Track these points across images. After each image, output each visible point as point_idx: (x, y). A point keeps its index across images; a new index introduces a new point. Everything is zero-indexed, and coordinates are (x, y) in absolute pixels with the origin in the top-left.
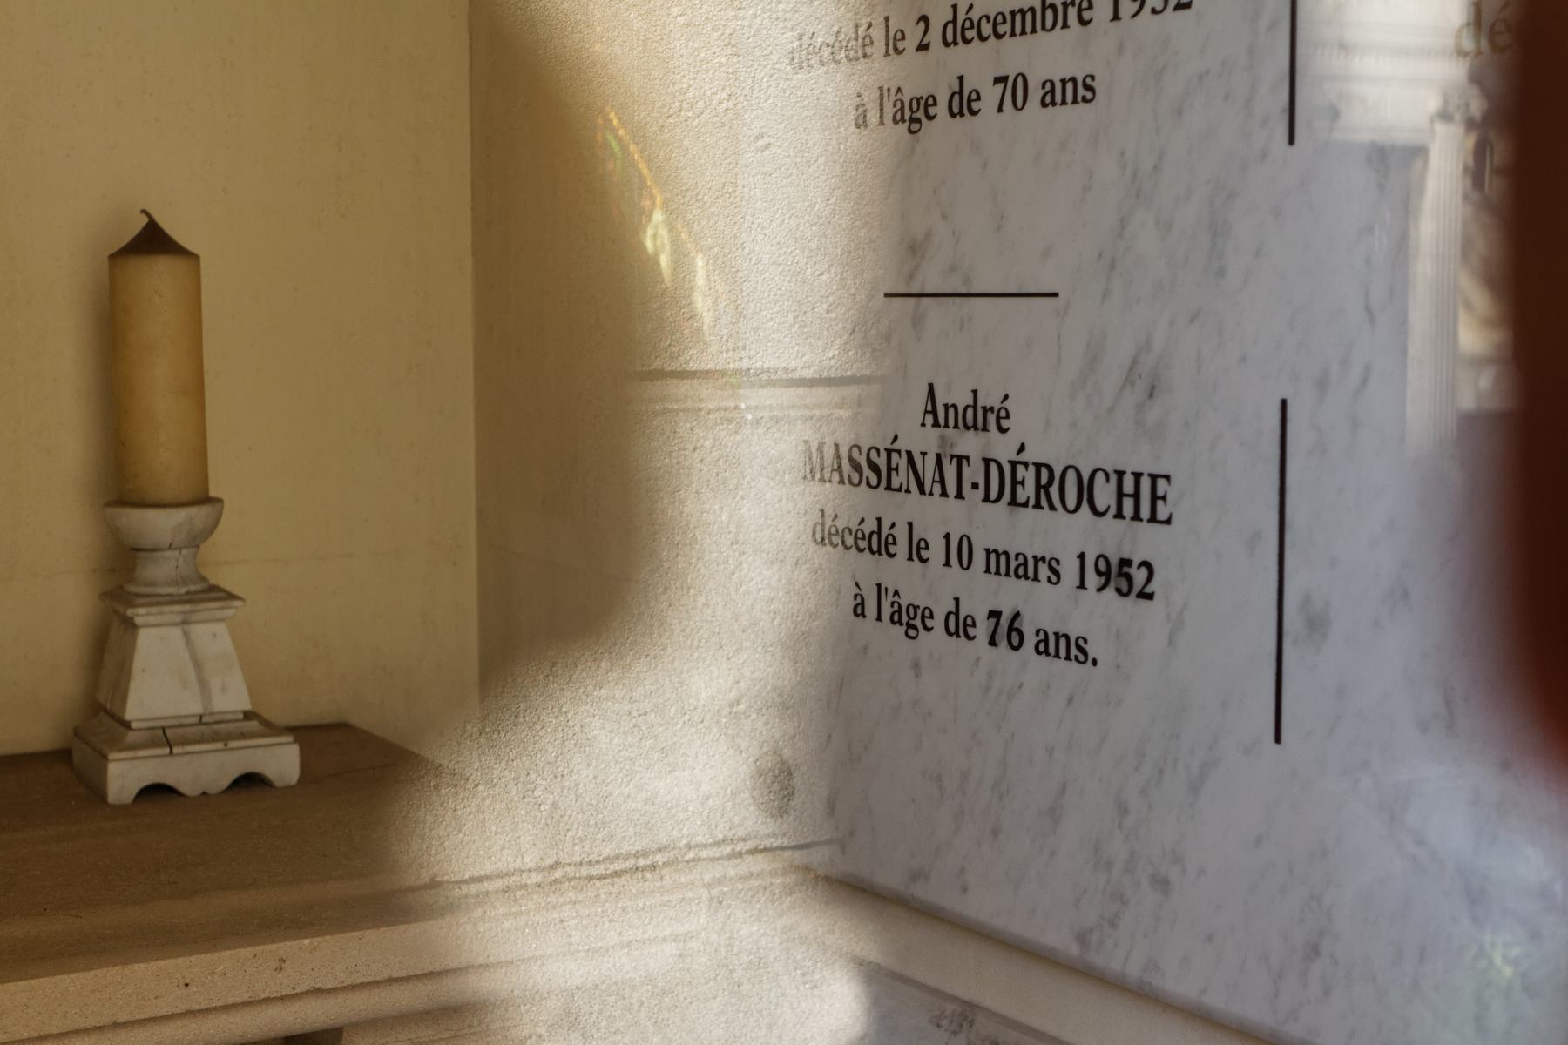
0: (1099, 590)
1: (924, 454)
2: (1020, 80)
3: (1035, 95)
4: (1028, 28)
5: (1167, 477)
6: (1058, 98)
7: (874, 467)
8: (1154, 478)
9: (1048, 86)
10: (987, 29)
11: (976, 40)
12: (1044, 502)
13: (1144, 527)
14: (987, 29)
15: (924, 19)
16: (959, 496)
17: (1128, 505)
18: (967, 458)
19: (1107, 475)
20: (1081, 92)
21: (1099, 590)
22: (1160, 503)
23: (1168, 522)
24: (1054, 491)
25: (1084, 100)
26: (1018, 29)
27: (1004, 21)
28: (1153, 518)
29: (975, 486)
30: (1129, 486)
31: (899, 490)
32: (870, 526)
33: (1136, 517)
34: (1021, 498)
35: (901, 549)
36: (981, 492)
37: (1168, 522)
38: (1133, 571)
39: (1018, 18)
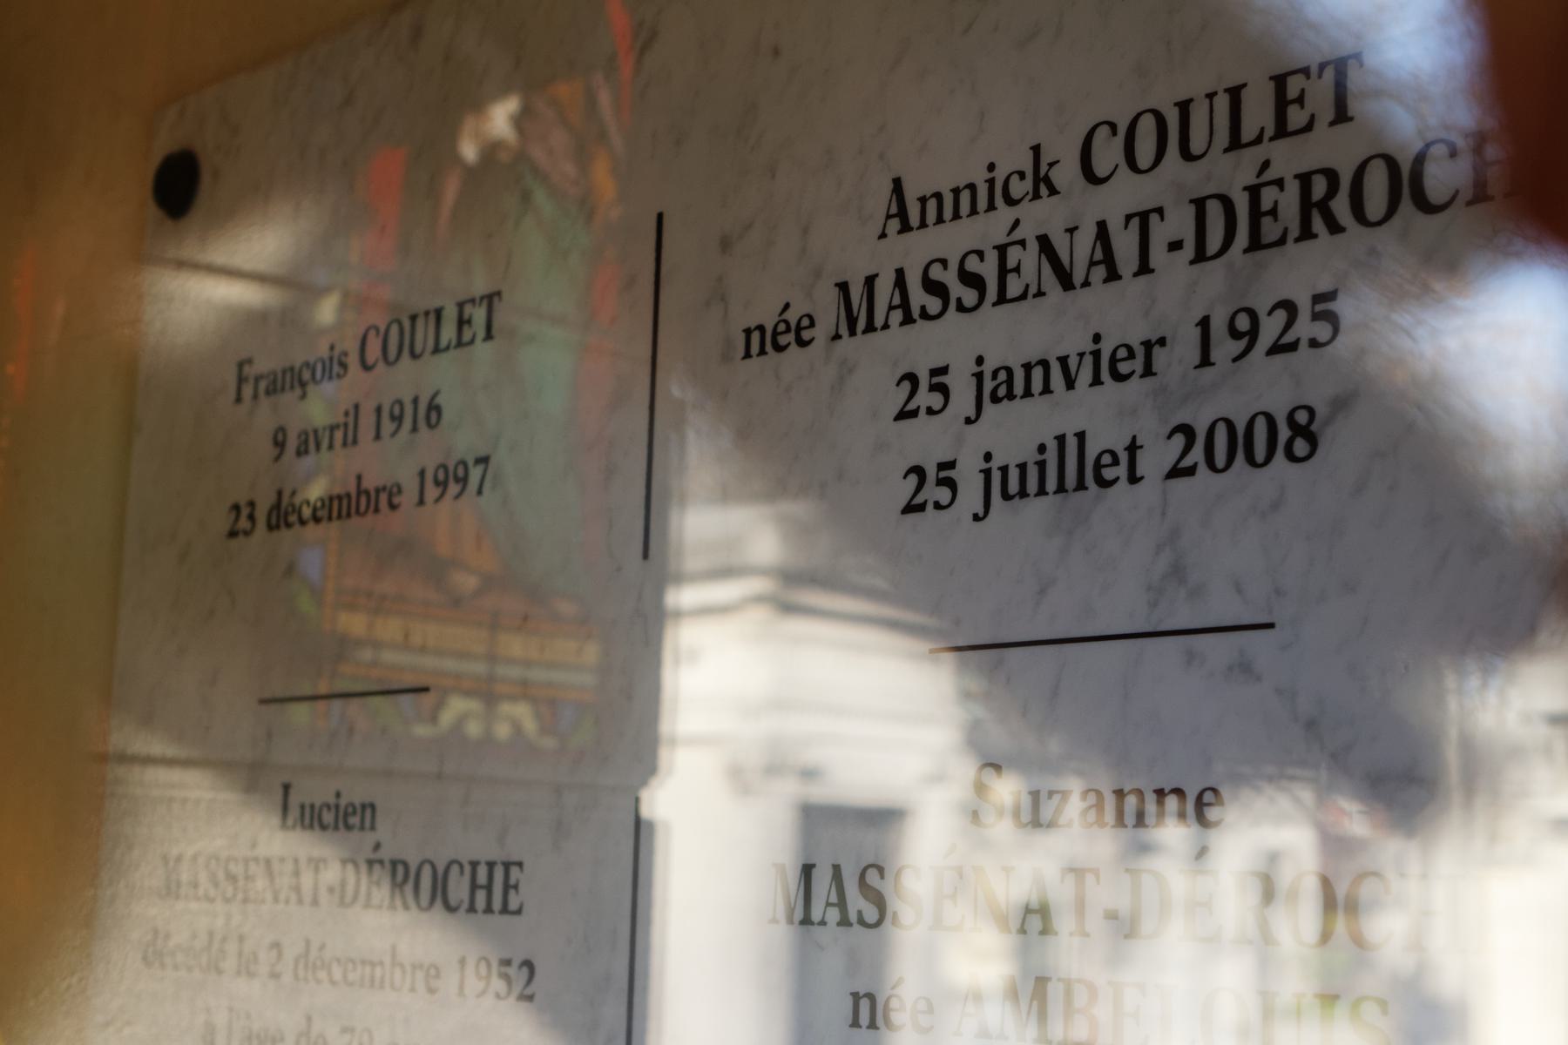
0: (479, 996)
5: (520, 864)
6: (1019, 388)
8: (507, 866)
11: (794, 346)
17: (481, 896)
18: (1160, 211)
19: (461, 866)
21: (479, 996)
23: (519, 912)
26: (335, 514)
28: (505, 910)
30: (482, 878)
33: (489, 910)
39: (336, 504)
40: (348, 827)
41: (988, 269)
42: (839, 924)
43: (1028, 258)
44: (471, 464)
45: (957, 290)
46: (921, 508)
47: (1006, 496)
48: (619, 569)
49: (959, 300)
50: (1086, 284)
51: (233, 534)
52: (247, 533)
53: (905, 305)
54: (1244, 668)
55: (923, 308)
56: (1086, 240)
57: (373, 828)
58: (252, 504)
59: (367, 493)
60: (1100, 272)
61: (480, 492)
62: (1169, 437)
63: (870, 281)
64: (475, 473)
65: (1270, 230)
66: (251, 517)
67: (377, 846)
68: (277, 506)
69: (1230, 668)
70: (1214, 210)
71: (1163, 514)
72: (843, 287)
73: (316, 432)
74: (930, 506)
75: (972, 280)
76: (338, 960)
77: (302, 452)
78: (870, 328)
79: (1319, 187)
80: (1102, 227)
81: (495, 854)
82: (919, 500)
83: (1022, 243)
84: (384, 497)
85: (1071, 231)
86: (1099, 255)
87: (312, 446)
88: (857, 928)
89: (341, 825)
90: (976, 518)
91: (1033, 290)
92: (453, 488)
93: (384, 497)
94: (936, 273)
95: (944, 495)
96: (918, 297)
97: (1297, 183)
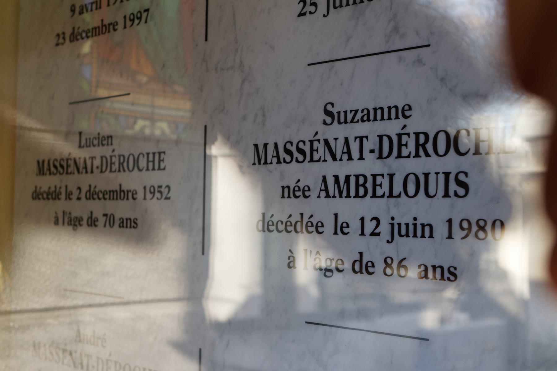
1: (336, 139)
2: (112, 217)
3: (117, 223)
4: (115, 197)
5: (164, 153)
7: (62, 166)
8: (160, 153)
9: (121, 220)
10: (101, 196)
12: (121, 169)
13: (157, 172)
14: (101, 196)
15: (79, 188)
16: (92, 172)
17: (151, 165)
18: (367, 137)
19: (143, 155)
20: (133, 224)
22: (162, 163)
23: (164, 169)
24: (125, 165)
25: (134, 227)
26: (94, 34)
27: (107, 194)
28: (159, 169)
29: (93, 367)
30: (151, 158)
31: (319, 161)
32: (53, 189)
34: (113, 169)
35: (63, 196)
36: (100, 170)
37: (164, 169)
38: (162, 189)
39: (94, 31)
40: (103, 145)
41: (307, 148)
42: (277, 163)
43: (321, 147)
44: (142, 12)
45: (296, 154)
46: (305, 14)
47: (335, 7)
48: (197, 45)
49: (297, 158)
50: (341, 160)
51: (57, 45)
52: (63, 44)
53: (278, 156)
54: (419, 61)
55: (284, 159)
56: (341, 141)
57: (112, 144)
58: (64, 33)
59: (105, 26)
60: (345, 157)
61: (146, 22)
62: (371, 221)
63: (266, 145)
64: (144, 15)
65: (405, 152)
66: (64, 38)
67: (113, 151)
68: (73, 33)
69: (414, 62)
70: (385, 140)
71: (391, 9)
72: (256, 146)
73: (86, 5)
74: (308, 13)
75: (301, 151)
76: (101, 192)
77: (81, 13)
78: (266, 163)
79: (422, 139)
80: (346, 140)
81: (156, 150)
82: (304, 11)
83: (319, 141)
84: (111, 27)
85: (336, 139)
86: (345, 150)
87: (85, 10)
88: (283, 164)
89: (93, 224)
90: (324, 16)
91: (322, 159)
92: (136, 21)
93: (111, 27)
94: (289, 146)
95: (313, 9)
96: (282, 154)
97: (414, 136)
